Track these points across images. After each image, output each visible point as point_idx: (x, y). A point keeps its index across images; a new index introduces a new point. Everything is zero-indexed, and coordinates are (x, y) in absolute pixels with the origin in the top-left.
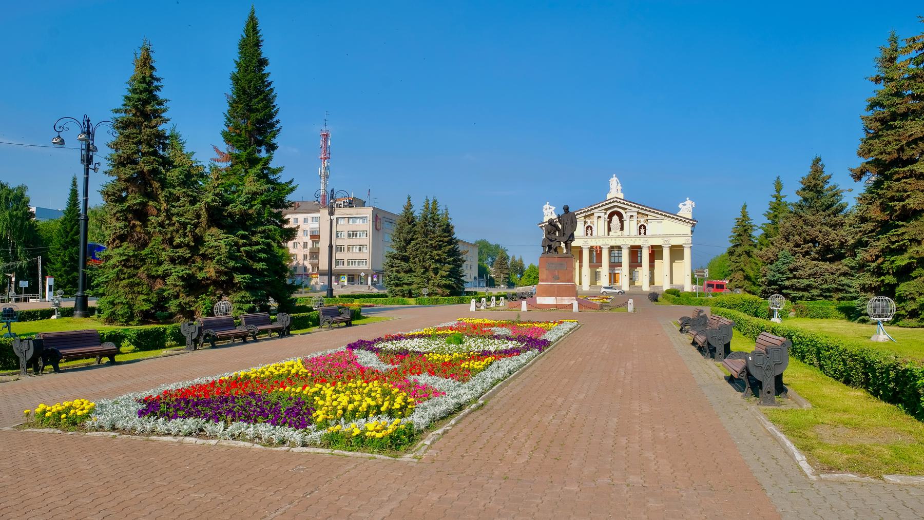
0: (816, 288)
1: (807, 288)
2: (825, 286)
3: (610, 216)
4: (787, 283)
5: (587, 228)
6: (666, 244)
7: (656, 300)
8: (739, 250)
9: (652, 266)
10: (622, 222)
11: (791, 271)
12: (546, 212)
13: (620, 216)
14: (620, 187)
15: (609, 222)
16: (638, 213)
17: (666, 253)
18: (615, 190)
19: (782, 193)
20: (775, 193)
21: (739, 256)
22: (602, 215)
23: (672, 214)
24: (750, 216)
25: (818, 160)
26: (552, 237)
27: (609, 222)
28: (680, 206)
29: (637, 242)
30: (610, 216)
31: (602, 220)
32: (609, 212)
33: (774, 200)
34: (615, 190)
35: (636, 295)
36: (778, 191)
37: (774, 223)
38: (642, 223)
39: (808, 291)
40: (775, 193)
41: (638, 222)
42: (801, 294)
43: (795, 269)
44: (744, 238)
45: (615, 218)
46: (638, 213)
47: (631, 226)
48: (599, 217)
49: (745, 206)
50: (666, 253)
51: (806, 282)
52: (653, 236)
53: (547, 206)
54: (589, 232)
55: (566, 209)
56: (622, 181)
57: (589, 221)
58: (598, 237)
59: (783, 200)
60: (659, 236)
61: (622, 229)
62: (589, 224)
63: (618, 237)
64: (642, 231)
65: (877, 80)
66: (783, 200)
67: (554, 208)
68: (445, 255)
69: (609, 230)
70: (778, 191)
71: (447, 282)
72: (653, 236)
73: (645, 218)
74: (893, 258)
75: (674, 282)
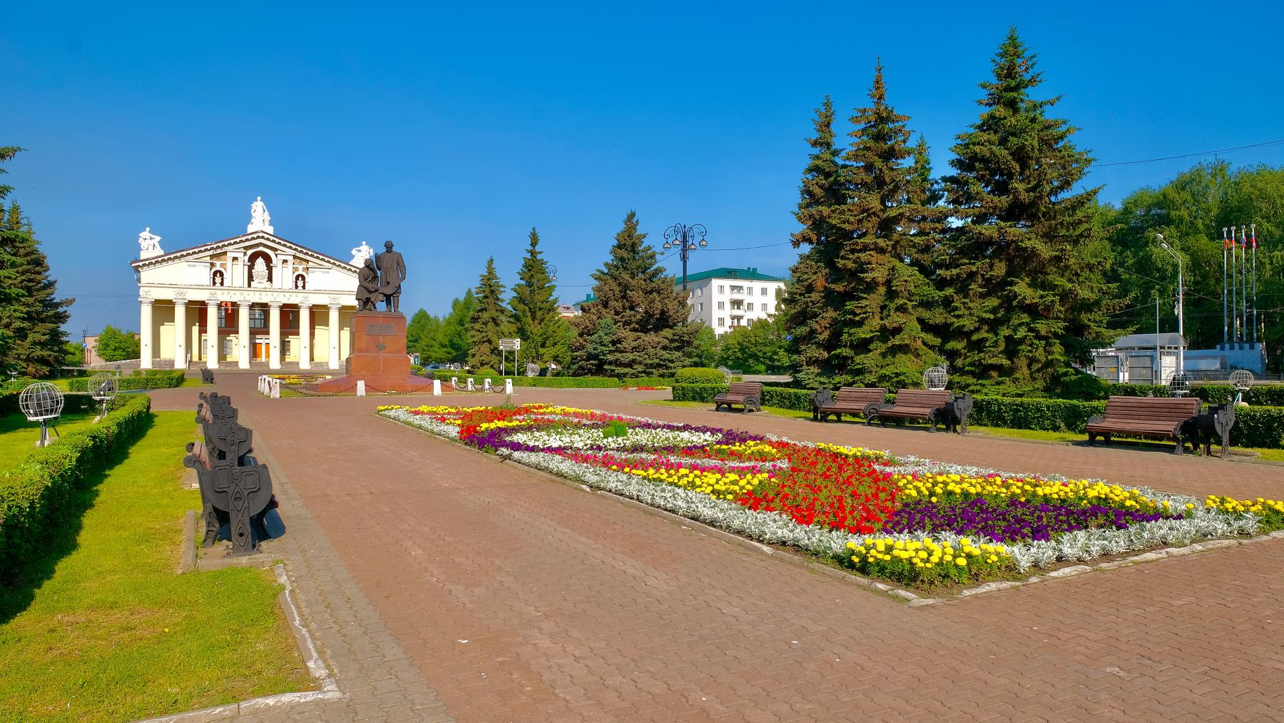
0: (640, 363)
1: (630, 364)
2: (649, 362)
3: (253, 258)
4: (610, 357)
5: (215, 274)
6: (180, 298)
7: (212, 381)
8: (485, 316)
9: (312, 335)
10: (270, 269)
11: (614, 343)
12: (144, 244)
13: (268, 260)
14: (267, 218)
15: (251, 268)
16: (295, 257)
17: (180, 312)
18: (260, 220)
19: (538, 249)
20: (530, 248)
21: (485, 324)
22: (240, 255)
23: (342, 261)
24: (498, 273)
25: (632, 215)
26: (371, 286)
27: (251, 268)
28: (354, 252)
29: (293, 300)
30: (253, 258)
31: (240, 263)
32: (250, 252)
33: (528, 256)
34: (260, 220)
35: (287, 374)
36: (534, 244)
37: (530, 285)
38: (300, 272)
39: (631, 367)
40: (530, 248)
41: (295, 269)
42: (626, 370)
43: (619, 341)
44: (491, 300)
45: (260, 262)
46: (295, 257)
47: (285, 276)
48: (235, 259)
49: (491, 261)
50: (180, 312)
51: (631, 356)
52: (317, 292)
53: (145, 234)
54: (218, 280)
55: (389, 247)
56: (270, 207)
57: (218, 263)
58: (231, 288)
59: (539, 257)
60: (172, 286)
61: (270, 279)
62: (218, 268)
63: (265, 290)
64: (300, 283)
65: (815, 144)
66: (539, 257)
67: (158, 238)
68: (39, 307)
69: (251, 278)
70: (534, 244)
71: (45, 353)
72: (317, 292)
73: (304, 265)
74: (853, 331)
75: (317, 359)
